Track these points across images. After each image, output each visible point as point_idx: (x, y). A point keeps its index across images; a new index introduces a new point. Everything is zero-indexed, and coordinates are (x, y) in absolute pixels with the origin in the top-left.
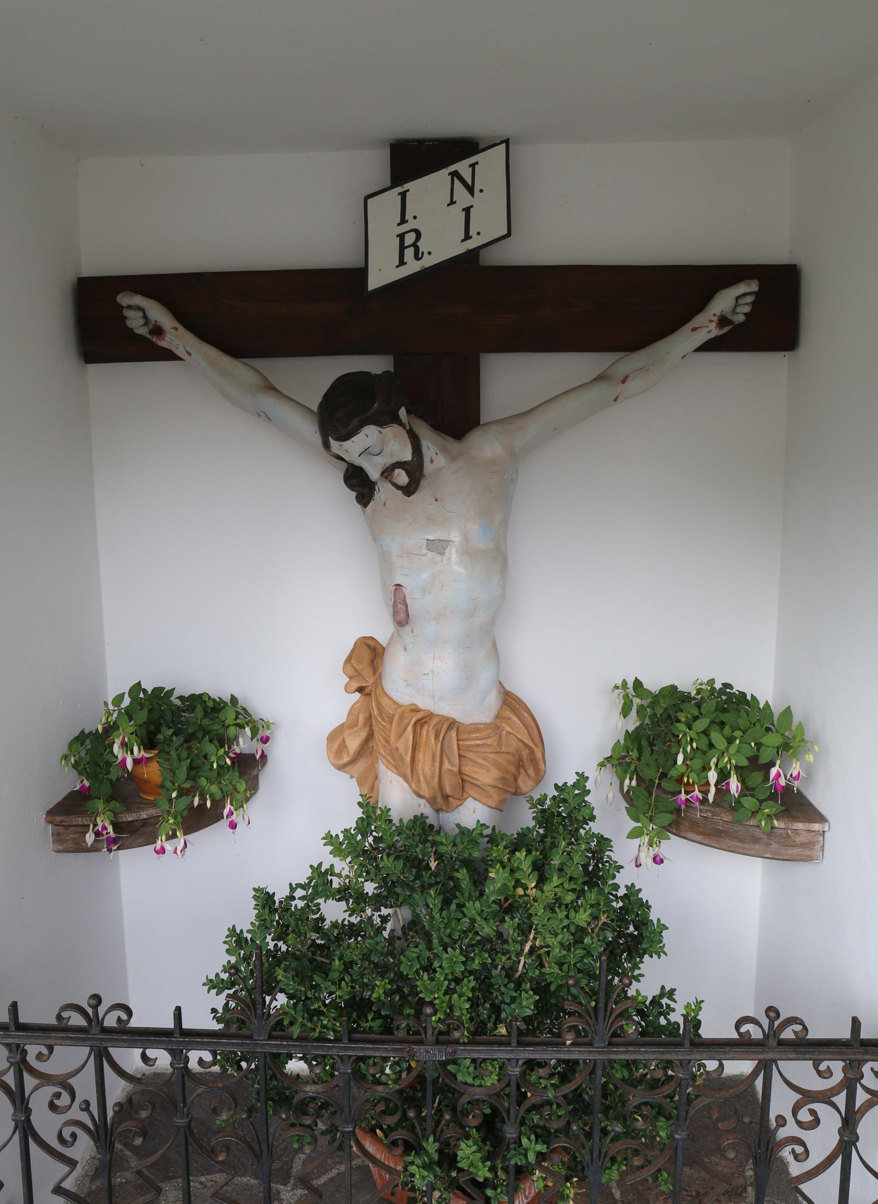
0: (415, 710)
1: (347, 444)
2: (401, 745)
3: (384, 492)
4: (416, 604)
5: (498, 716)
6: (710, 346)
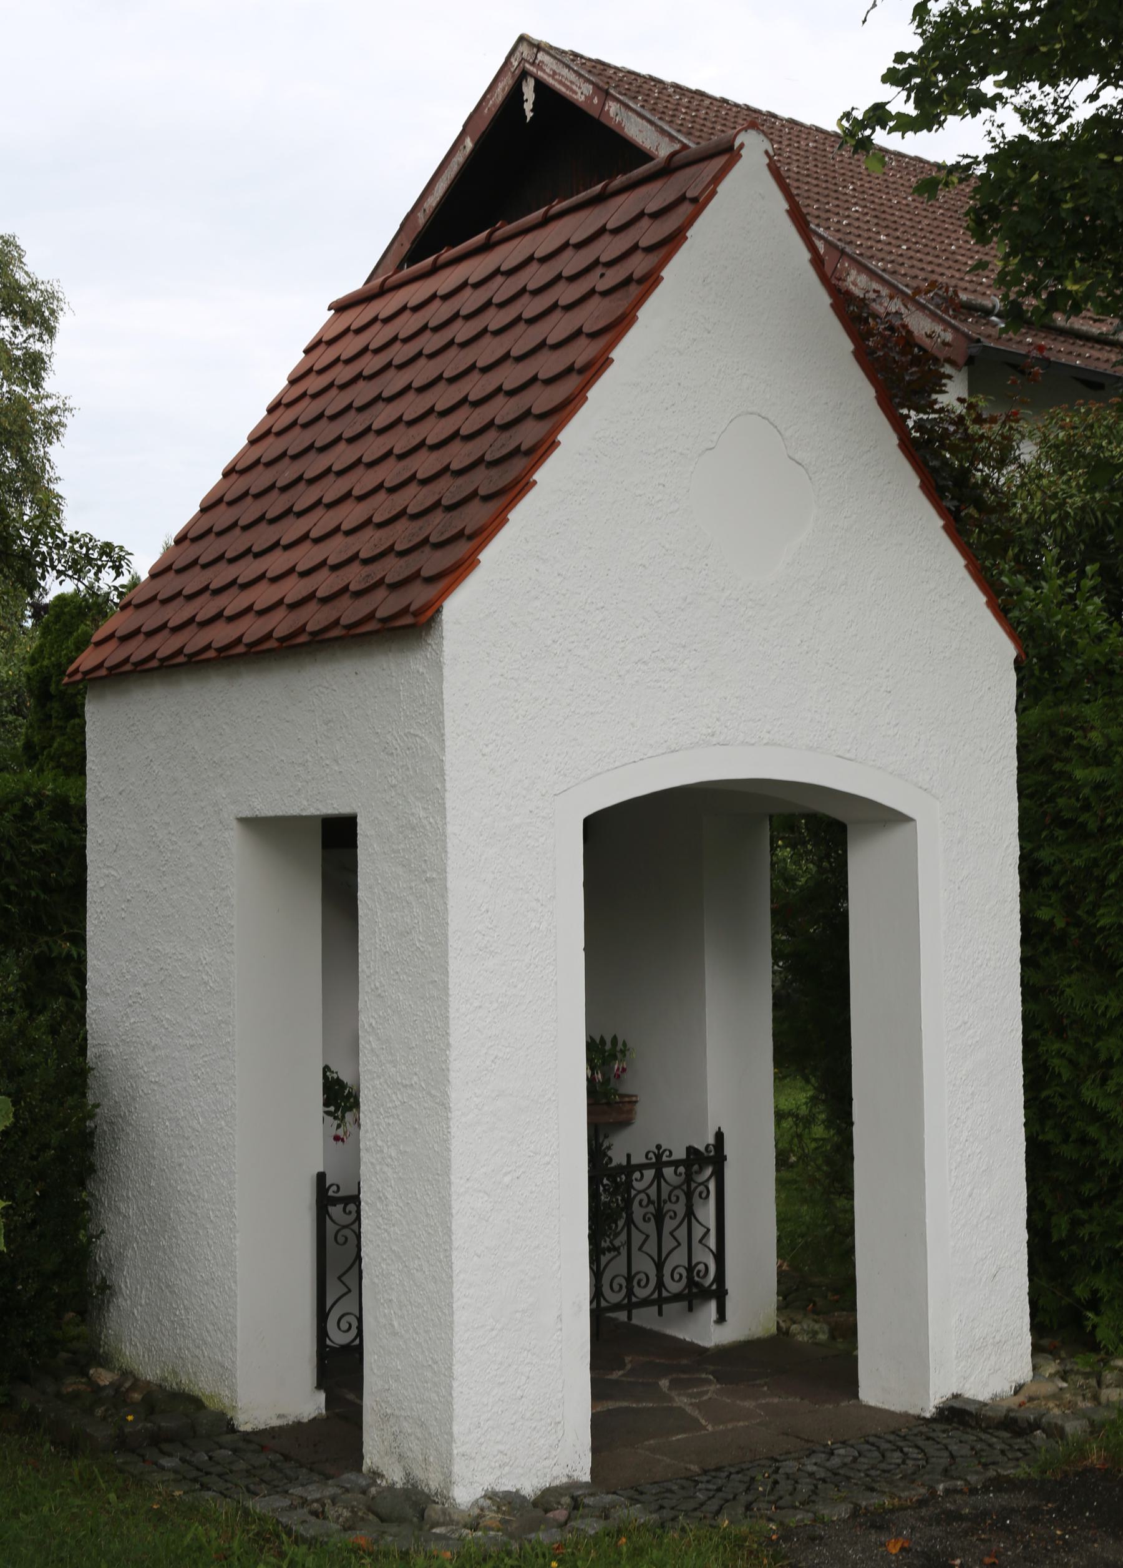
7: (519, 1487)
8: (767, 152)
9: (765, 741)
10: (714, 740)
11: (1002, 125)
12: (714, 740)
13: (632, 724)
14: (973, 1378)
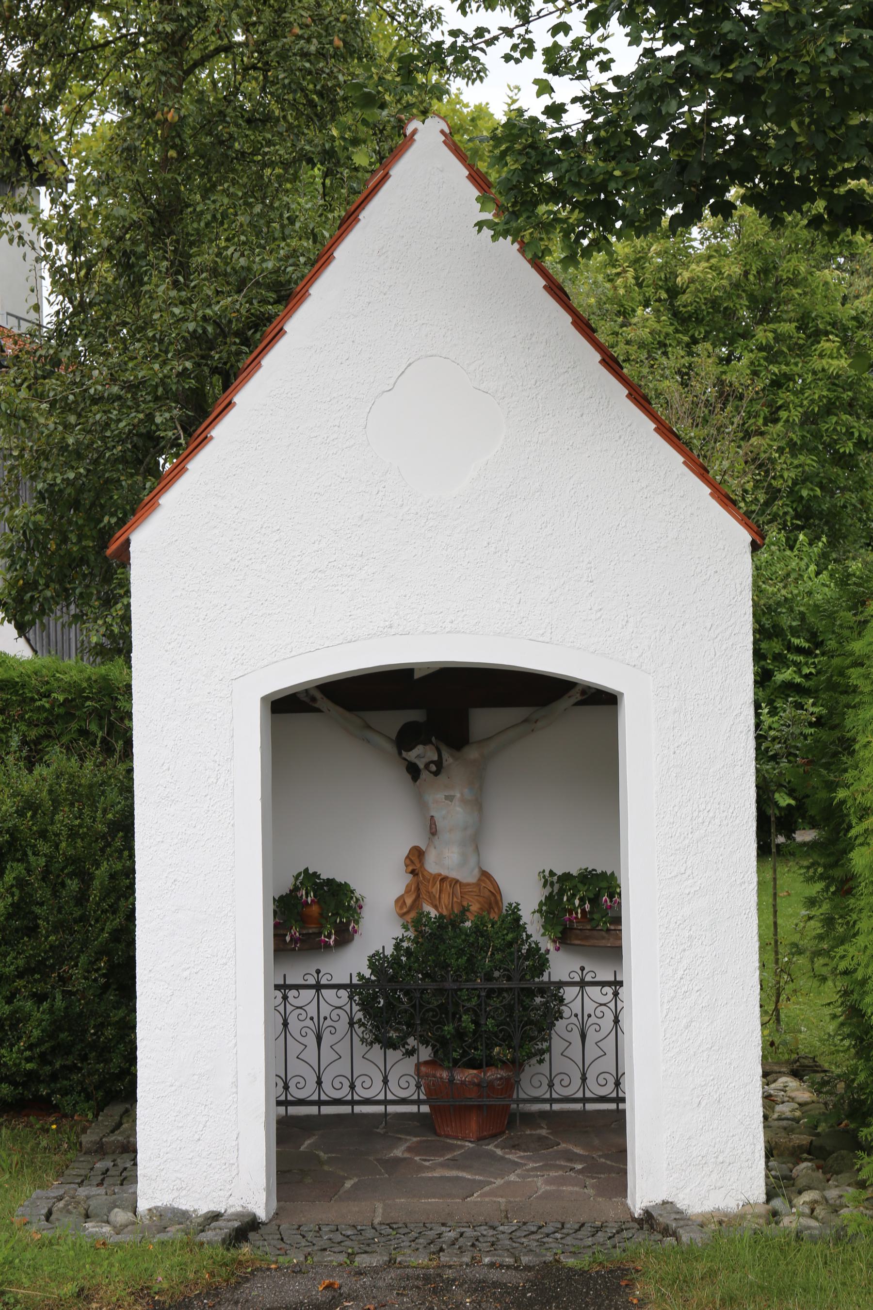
0: (440, 875)
1: (410, 753)
2: (434, 890)
3: (425, 775)
4: (440, 824)
5: (479, 880)
6: (578, 704)
7: (196, 1207)
8: (442, 132)
9: (447, 630)
10: (393, 631)
11: (509, 86)
12: (393, 631)
13: (310, 622)
14: (688, 1190)
